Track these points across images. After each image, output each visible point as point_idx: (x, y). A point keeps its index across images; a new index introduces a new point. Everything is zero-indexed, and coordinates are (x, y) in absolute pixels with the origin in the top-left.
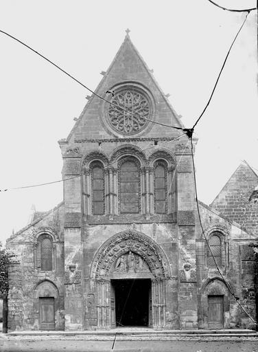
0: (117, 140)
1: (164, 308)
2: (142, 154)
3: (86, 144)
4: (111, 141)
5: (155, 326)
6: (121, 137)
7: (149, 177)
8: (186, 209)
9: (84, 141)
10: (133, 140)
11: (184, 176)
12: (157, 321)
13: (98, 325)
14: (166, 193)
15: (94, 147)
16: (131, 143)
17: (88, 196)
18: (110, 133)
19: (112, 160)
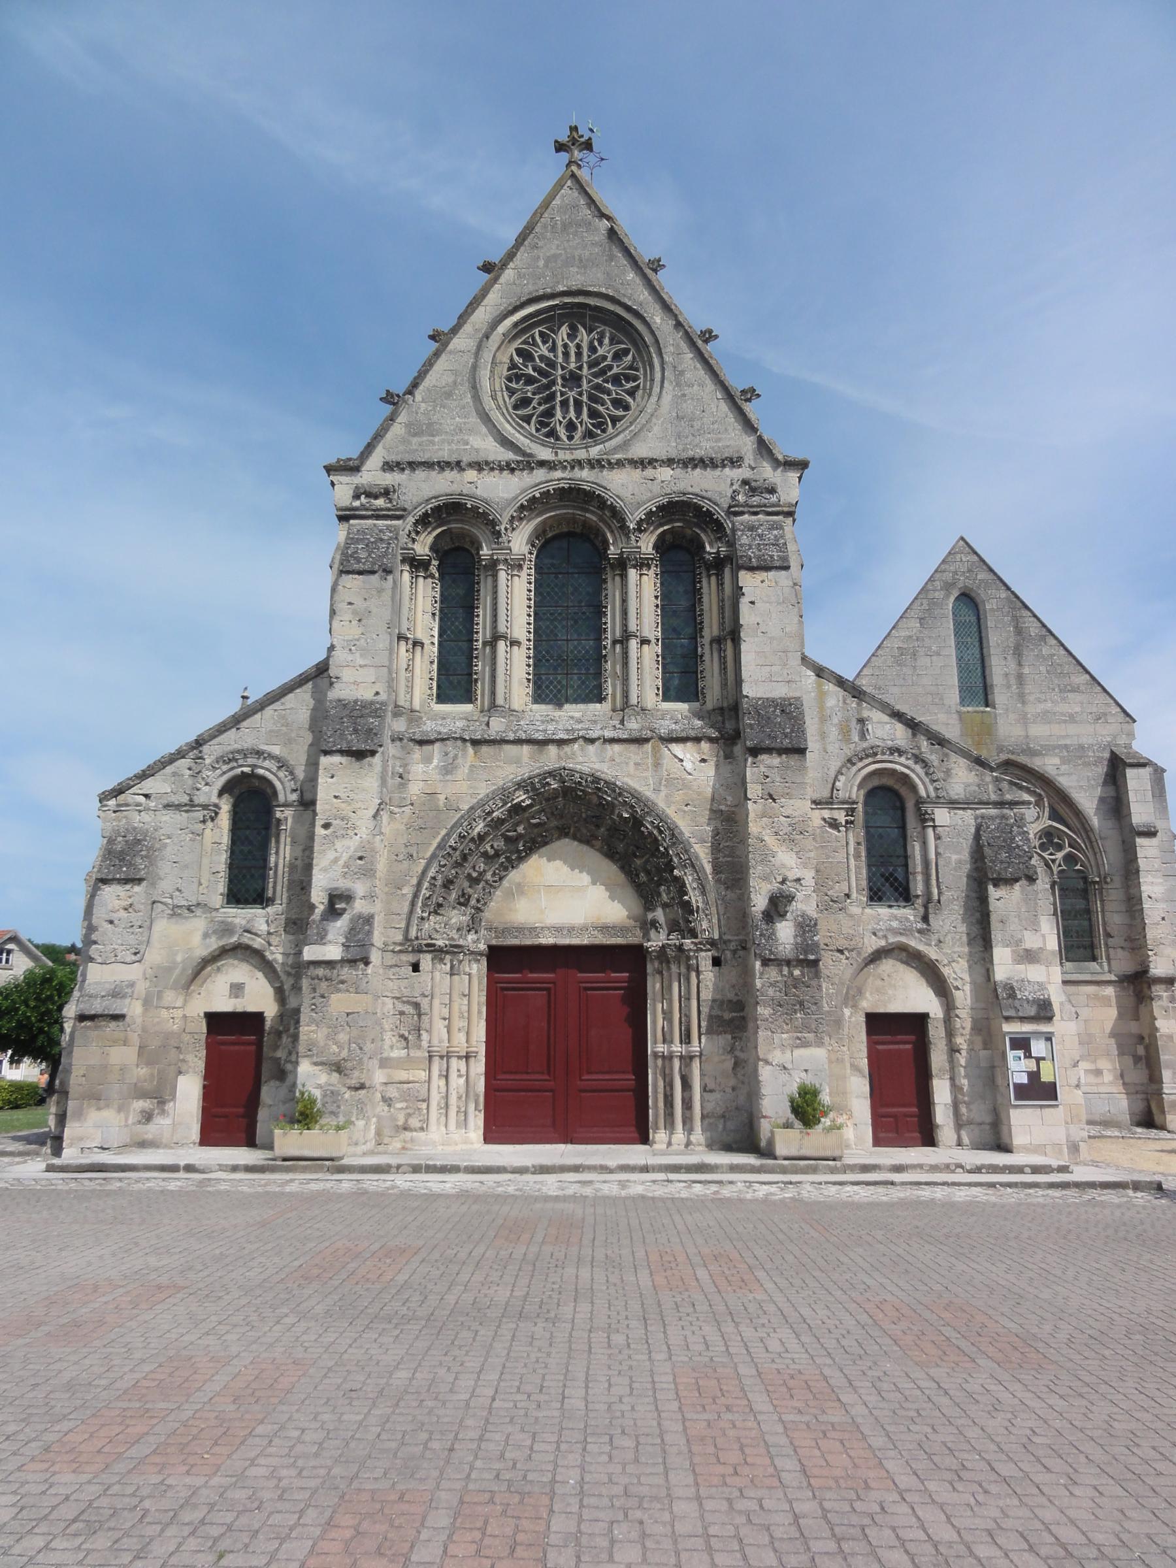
0: (529, 463)
1: (696, 1064)
2: (616, 515)
3: (420, 474)
4: (509, 467)
5: (660, 1136)
6: (545, 454)
7: (639, 585)
8: (779, 691)
9: (413, 465)
10: (595, 464)
11: (1102, 1109)
12: (670, 1124)
13: (433, 1126)
14: (698, 655)
15: (442, 485)
16: (585, 474)
17: (417, 643)
18: (506, 442)
19: (639, 530)
